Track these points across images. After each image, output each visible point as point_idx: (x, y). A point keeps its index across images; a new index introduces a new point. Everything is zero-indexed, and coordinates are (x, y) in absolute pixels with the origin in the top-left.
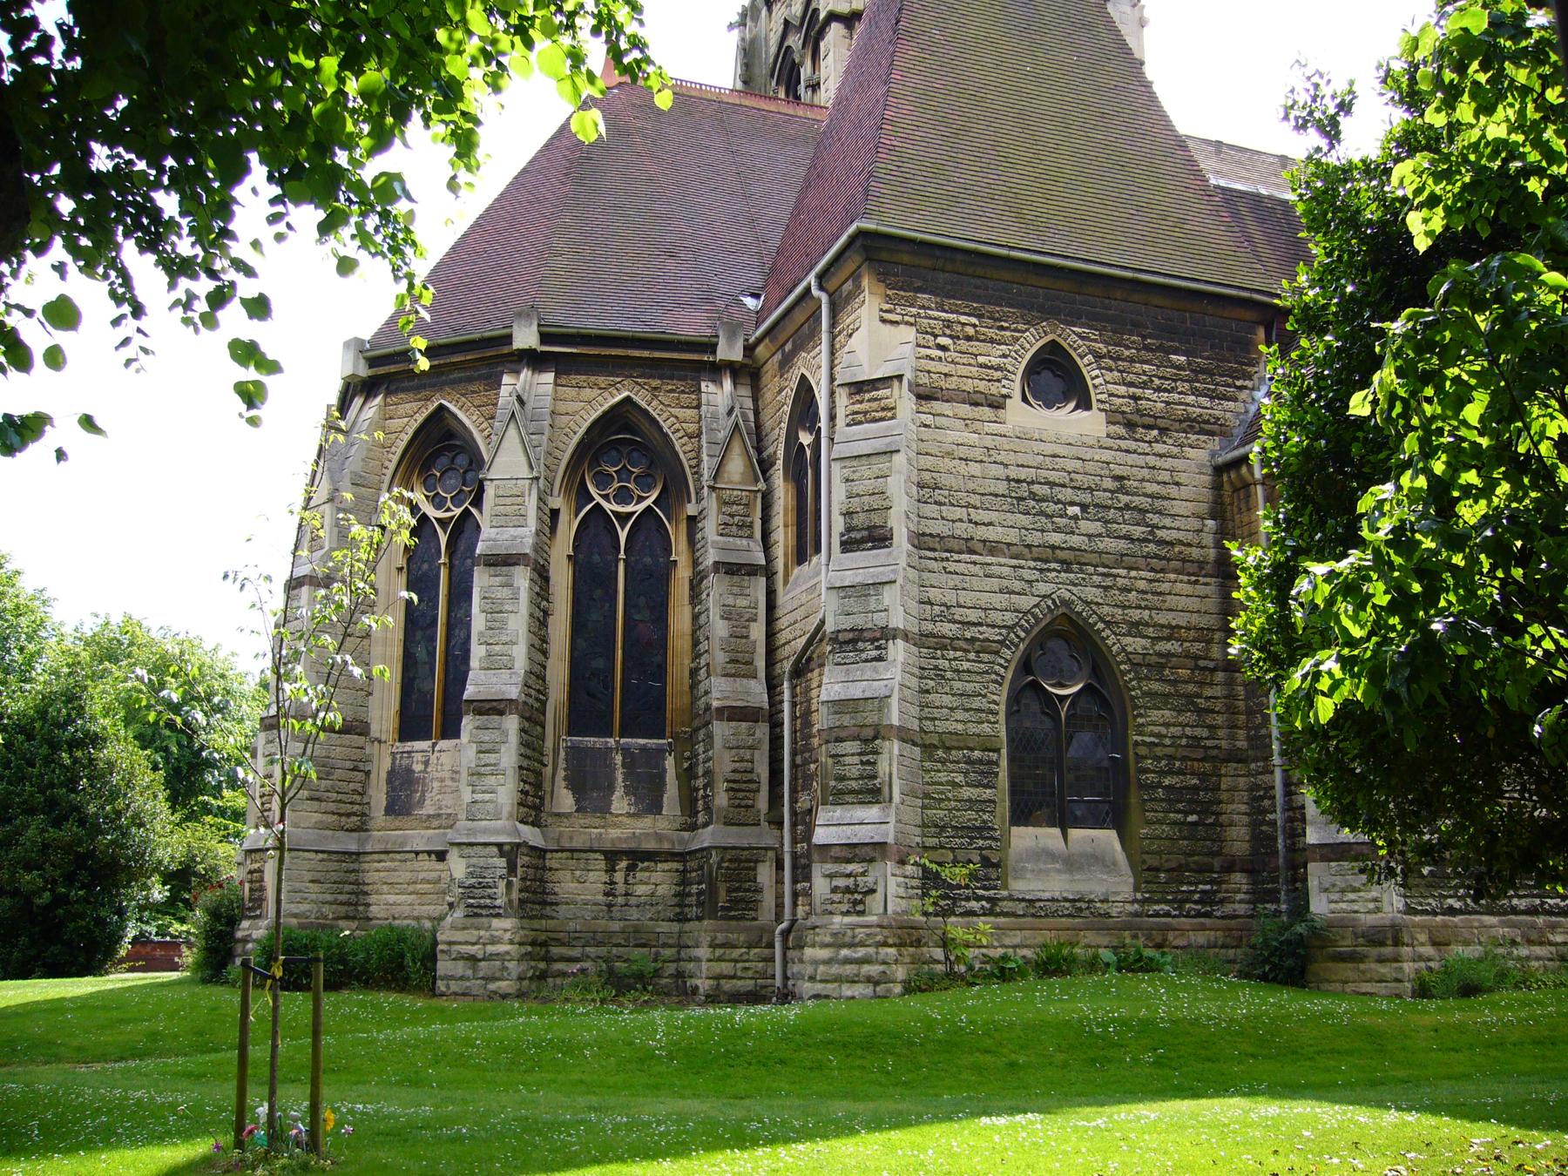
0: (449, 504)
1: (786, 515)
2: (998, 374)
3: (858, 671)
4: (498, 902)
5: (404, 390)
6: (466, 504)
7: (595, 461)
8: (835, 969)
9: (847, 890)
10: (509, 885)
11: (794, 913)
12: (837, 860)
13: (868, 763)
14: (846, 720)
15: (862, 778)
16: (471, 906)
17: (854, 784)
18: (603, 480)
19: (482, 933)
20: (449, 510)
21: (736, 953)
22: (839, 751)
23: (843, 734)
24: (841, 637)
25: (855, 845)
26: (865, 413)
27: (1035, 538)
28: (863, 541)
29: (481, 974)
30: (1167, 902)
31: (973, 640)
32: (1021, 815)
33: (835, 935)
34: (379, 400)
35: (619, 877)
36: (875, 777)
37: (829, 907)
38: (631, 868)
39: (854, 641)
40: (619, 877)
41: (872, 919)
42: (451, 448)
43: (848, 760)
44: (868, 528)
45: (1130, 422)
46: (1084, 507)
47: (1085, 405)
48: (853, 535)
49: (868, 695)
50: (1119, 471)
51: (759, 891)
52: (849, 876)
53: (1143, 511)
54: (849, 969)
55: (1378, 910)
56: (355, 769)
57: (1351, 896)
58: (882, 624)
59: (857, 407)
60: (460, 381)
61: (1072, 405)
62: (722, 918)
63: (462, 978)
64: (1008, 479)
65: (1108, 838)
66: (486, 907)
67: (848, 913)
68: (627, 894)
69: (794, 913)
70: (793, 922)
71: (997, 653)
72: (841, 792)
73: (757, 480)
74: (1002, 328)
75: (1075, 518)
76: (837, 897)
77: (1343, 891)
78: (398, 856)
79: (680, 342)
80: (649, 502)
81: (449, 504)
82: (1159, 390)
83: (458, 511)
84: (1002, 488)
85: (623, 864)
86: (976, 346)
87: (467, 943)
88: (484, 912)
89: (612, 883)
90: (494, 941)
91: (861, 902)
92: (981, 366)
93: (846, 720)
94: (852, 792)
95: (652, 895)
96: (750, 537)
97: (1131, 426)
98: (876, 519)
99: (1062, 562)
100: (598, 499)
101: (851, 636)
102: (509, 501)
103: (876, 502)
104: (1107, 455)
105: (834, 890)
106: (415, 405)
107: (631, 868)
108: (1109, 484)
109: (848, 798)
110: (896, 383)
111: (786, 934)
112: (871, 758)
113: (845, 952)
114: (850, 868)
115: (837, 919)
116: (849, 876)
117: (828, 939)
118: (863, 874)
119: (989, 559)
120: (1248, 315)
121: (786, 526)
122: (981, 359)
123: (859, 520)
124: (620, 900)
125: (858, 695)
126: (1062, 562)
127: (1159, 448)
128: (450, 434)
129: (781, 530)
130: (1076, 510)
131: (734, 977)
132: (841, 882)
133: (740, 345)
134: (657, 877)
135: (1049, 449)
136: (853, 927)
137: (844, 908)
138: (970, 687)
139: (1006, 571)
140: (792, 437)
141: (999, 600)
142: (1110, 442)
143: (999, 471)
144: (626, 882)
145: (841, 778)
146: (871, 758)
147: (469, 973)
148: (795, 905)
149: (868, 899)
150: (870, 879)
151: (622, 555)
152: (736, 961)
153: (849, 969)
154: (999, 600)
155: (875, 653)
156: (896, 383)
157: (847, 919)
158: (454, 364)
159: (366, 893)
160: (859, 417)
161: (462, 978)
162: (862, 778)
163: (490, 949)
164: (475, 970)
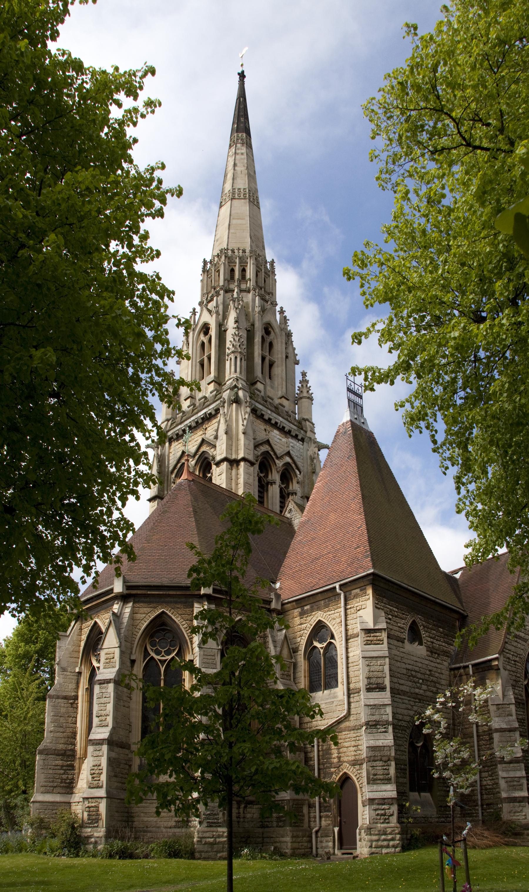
0: (163, 653)
1: (305, 672)
2: (403, 630)
3: (377, 736)
4: (220, 821)
5: (142, 602)
6: (173, 655)
7: (152, 636)
8: (380, 843)
9: (382, 815)
10: (224, 814)
11: (320, 824)
12: (378, 804)
13: (386, 769)
14: (378, 754)
15: (383, 774)
16: (208, 822)
17: (381, 777)
18: (153, 645)
19: (214, 833)
20: (163, 656)
21: (299, 839)
22: (374, 765)
23: (376, 758)
24: (370, 723)
25: (384, 799)
26: (372, 641)
27: (412, 690)
28: (375, 688)
29: (215, 850)
30: (443, 817)
31: (401, 726)
32: (412, 789)
33: (379, 831)
34: (130, 604)
35: (241, 810)
36: (389, 774)
37: (376, 821)
38: (245, 807)
39: (375, 725)
40: (241, 810)
41: (392, 825)
42: (164, 630)
43: (378, 768)
44: (377, 684)
45: (432, 651)
46: (423, 680)
47: (421, 644)
48: (371, 686)
49: (385, 745)
50: (430, 668)
51: (303, 816)
52: (383, 810)
53: (435, 683)
54: (385, 843)
55: (526, 818)
56: (126, 764)
57: (518, 814)
58: (385, 719)
59: (368, 638)
60: (171, 602)
61: (417, 643)
62: (294, 826)
63: (207, 852)
64: (406, 669)
65: (428, 795)
66: (214, 823)
67: (383, 823)
68: (244, 817)
69: (320, 824)
70: (320, 827)
71: (405, 731)
72: (377, 780)
73: (292, 658)
74: (403, 614)
75: (421, 684)
76: (379, 817)
77: (514, 813)
78: (149, 801)
79: (154, 586)
80: (173, 655)
81: (163, 653)
82: (437, 640)
83: (170, 657)
84: (405, 671)
85: (243, 806)
86: (398, 620)
87: (208, 837)
88: (214, 825)
89: (239, 813)
90: (219, 836)
91: (388, 819)
92: (399, 627)
93: (378, 754)
94: (380, 780)
95: (252, 818)
96: (290, 680)
97: (432, 652)
98: (380, 681)
99: (419, 699)
100: (153, 654)
101: (374, 723)
102: (209, 657)
103: (380, 674)
104: (427, 662)
105: (378, 815)
106: (149, 610)
107: (245, 807)
108: (428, 672)
109: (379, 782)
110: (383, 631)
111: (317, 832)
112: (387, 768)
113: (383, 837)
114: (383, 807)
115: (379, 825)
116: (383, 810)
117: (376, 832)
118: (388, 809)
119: (403, 697)
120: (456, 616)
121: (305, 677)
122: (399, 625)
123: (373, 681)
124: (242, 820)
125: (381, 744)
126: (419, 699)
127: (438, 661)
128: (164, 624)
129: (303, 678)
130: (421, 681)
131: (299, 849)
132: (379, 812)
133: (280, 604)
134: (254, 811)
135: (415, 659)
136: (386, 828)
137: (382, 821)
138: (401, 742)
139: (407, 701)
140: (309, 642)
141: (405, 712)
142: (427, 658)
143: (404, 666)
144: (244, 813)
145: (375, 775)
146: (387, 768)
147: (210, 849)
148: (320, 821)
149: (391, 818)
150: (391, 811)
151: (162, 677)
152: (299, 842)
153: (385, 843)
154: (405, 712)
155: (384, 730)
156: (383, 631)
157: (382, 825)
158: (169, 595)
159: (133, 817)
160: (369, 642)
161: (207, 852)
162: (383, 774)
163: (218, 840)
164: (212, 848)
